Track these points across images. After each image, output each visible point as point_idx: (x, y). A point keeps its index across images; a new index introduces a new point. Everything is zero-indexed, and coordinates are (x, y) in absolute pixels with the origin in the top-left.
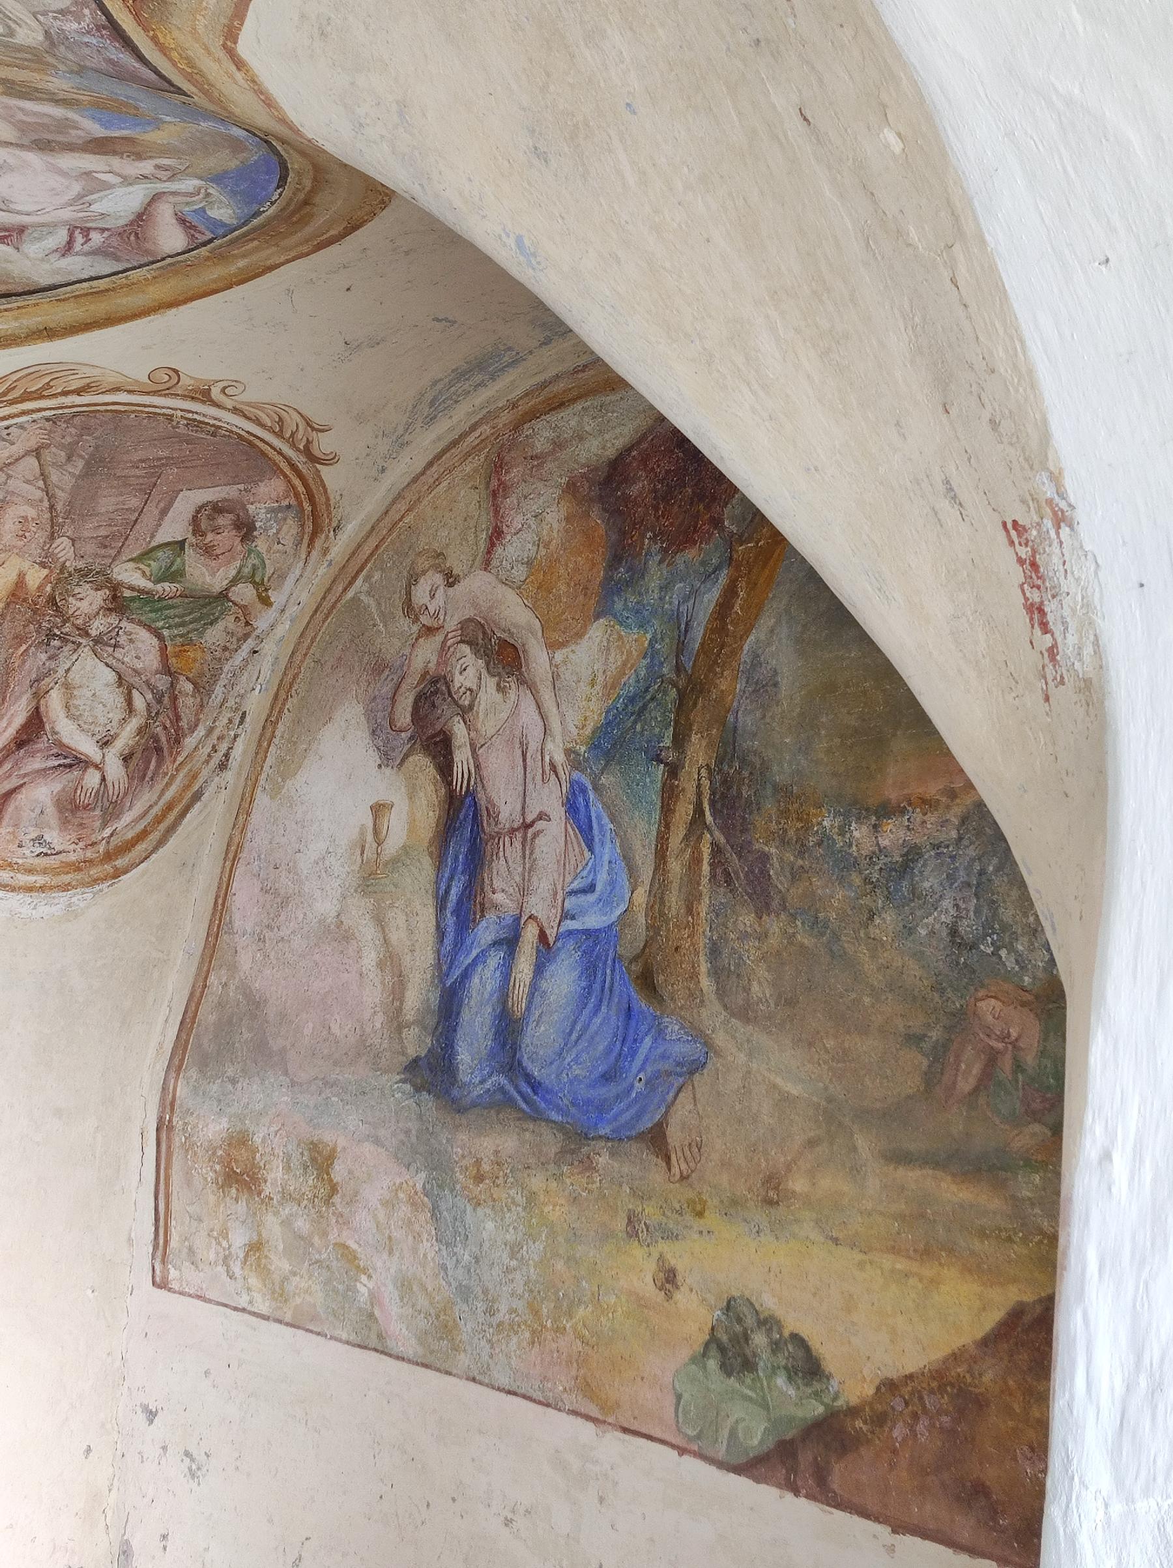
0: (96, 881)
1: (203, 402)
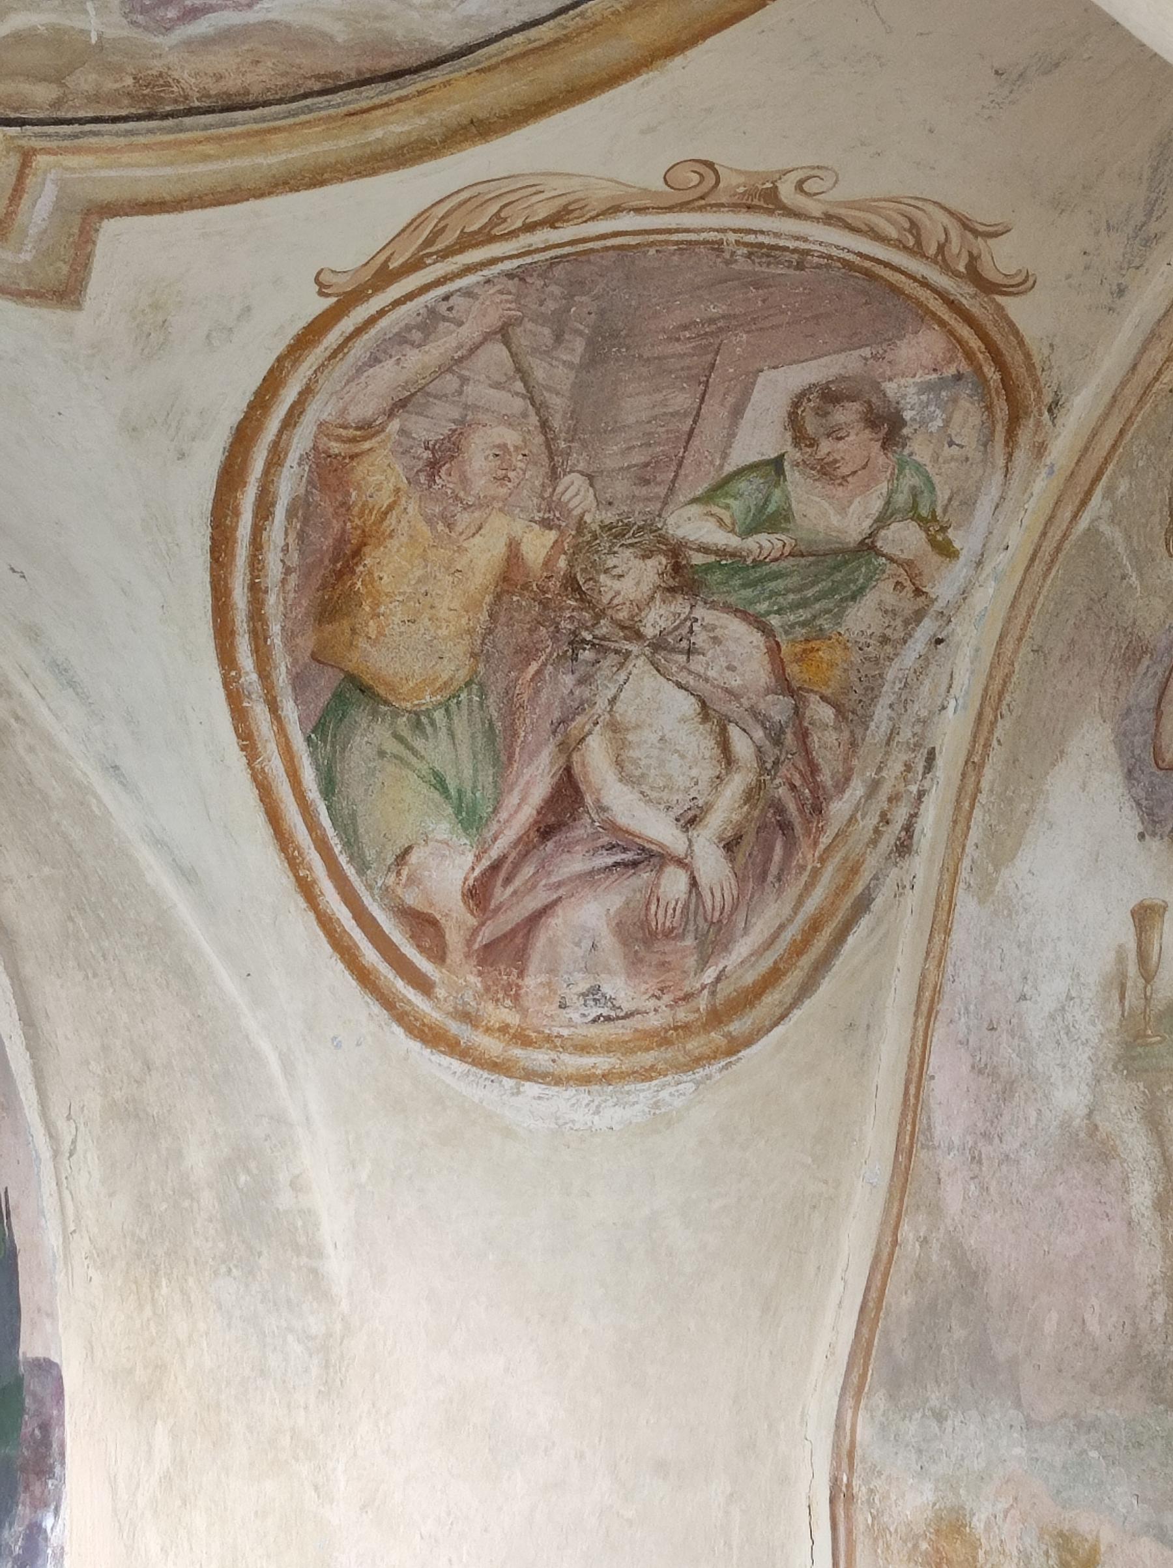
0: (698, 1061)
1: (770, 212)
